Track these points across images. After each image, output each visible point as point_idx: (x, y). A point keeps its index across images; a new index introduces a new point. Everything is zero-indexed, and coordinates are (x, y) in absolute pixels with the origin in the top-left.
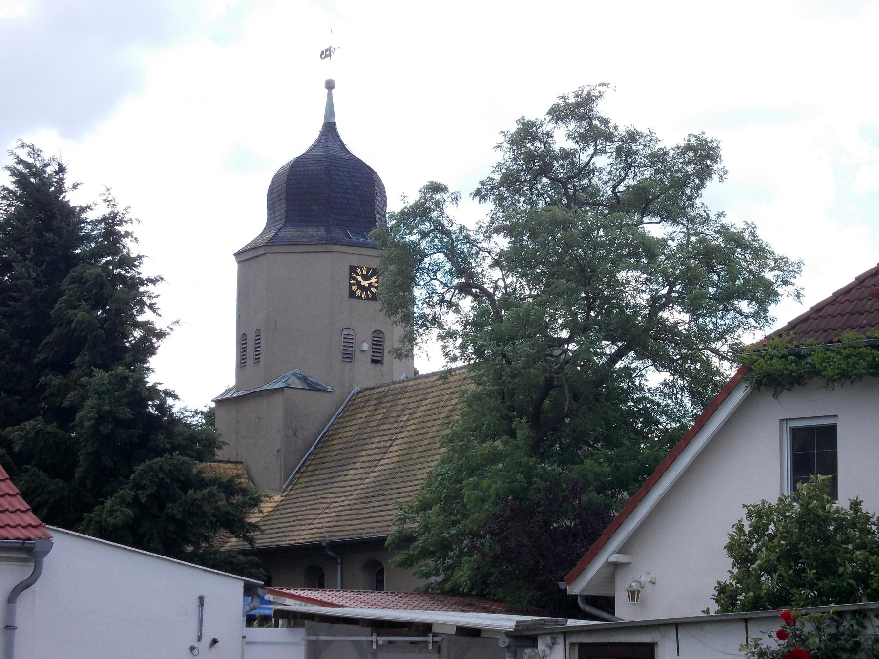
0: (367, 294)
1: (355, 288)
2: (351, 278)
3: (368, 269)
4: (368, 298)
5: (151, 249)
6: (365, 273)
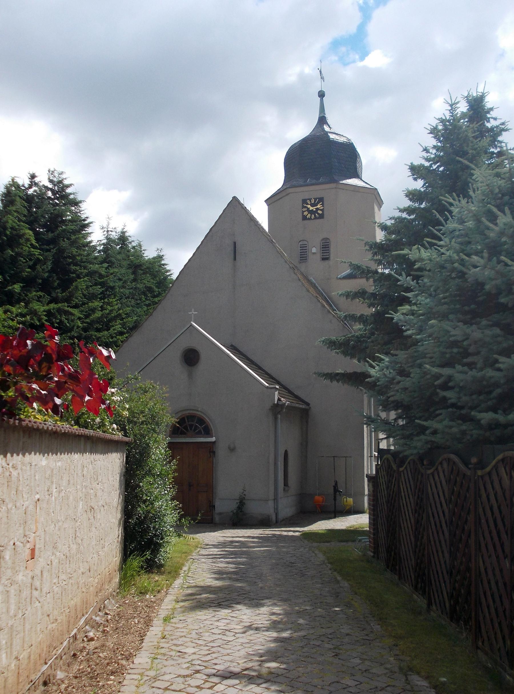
0: (315, 215)
1: (306, 213)
2: (304, 207)
3: (315, 199)
4: (316, 218)
5: (423, 163)
6: (313, 202)
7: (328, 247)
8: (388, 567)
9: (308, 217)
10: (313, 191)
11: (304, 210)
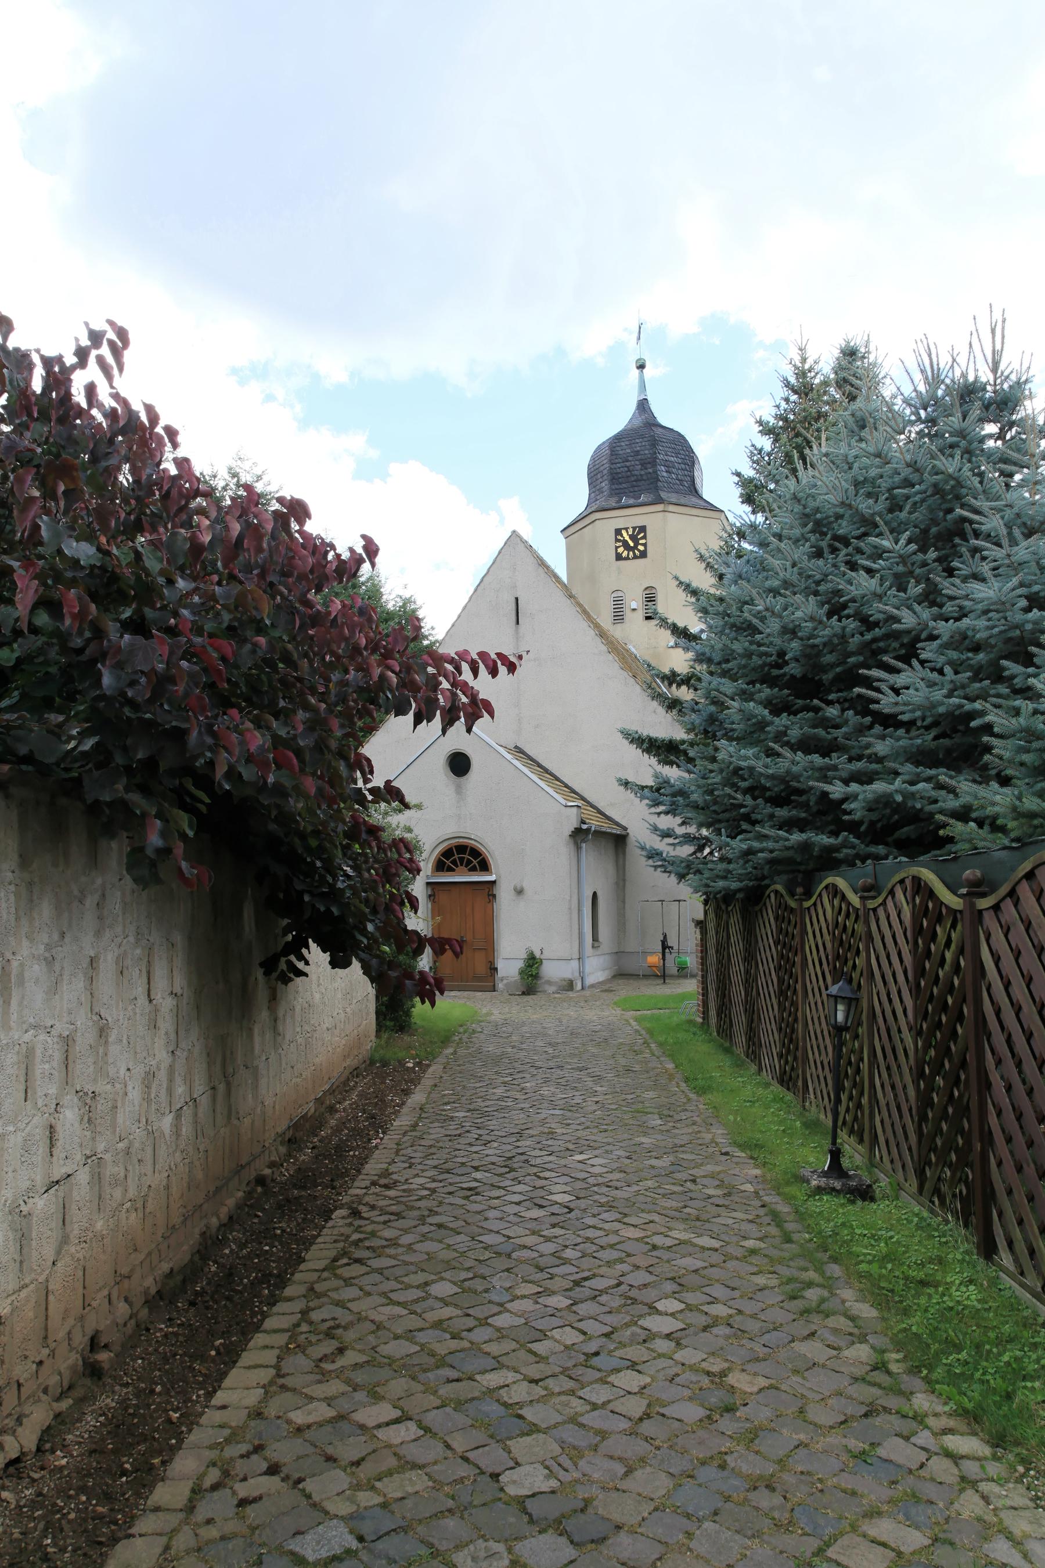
4: (635, 557)
10: (629, 519)
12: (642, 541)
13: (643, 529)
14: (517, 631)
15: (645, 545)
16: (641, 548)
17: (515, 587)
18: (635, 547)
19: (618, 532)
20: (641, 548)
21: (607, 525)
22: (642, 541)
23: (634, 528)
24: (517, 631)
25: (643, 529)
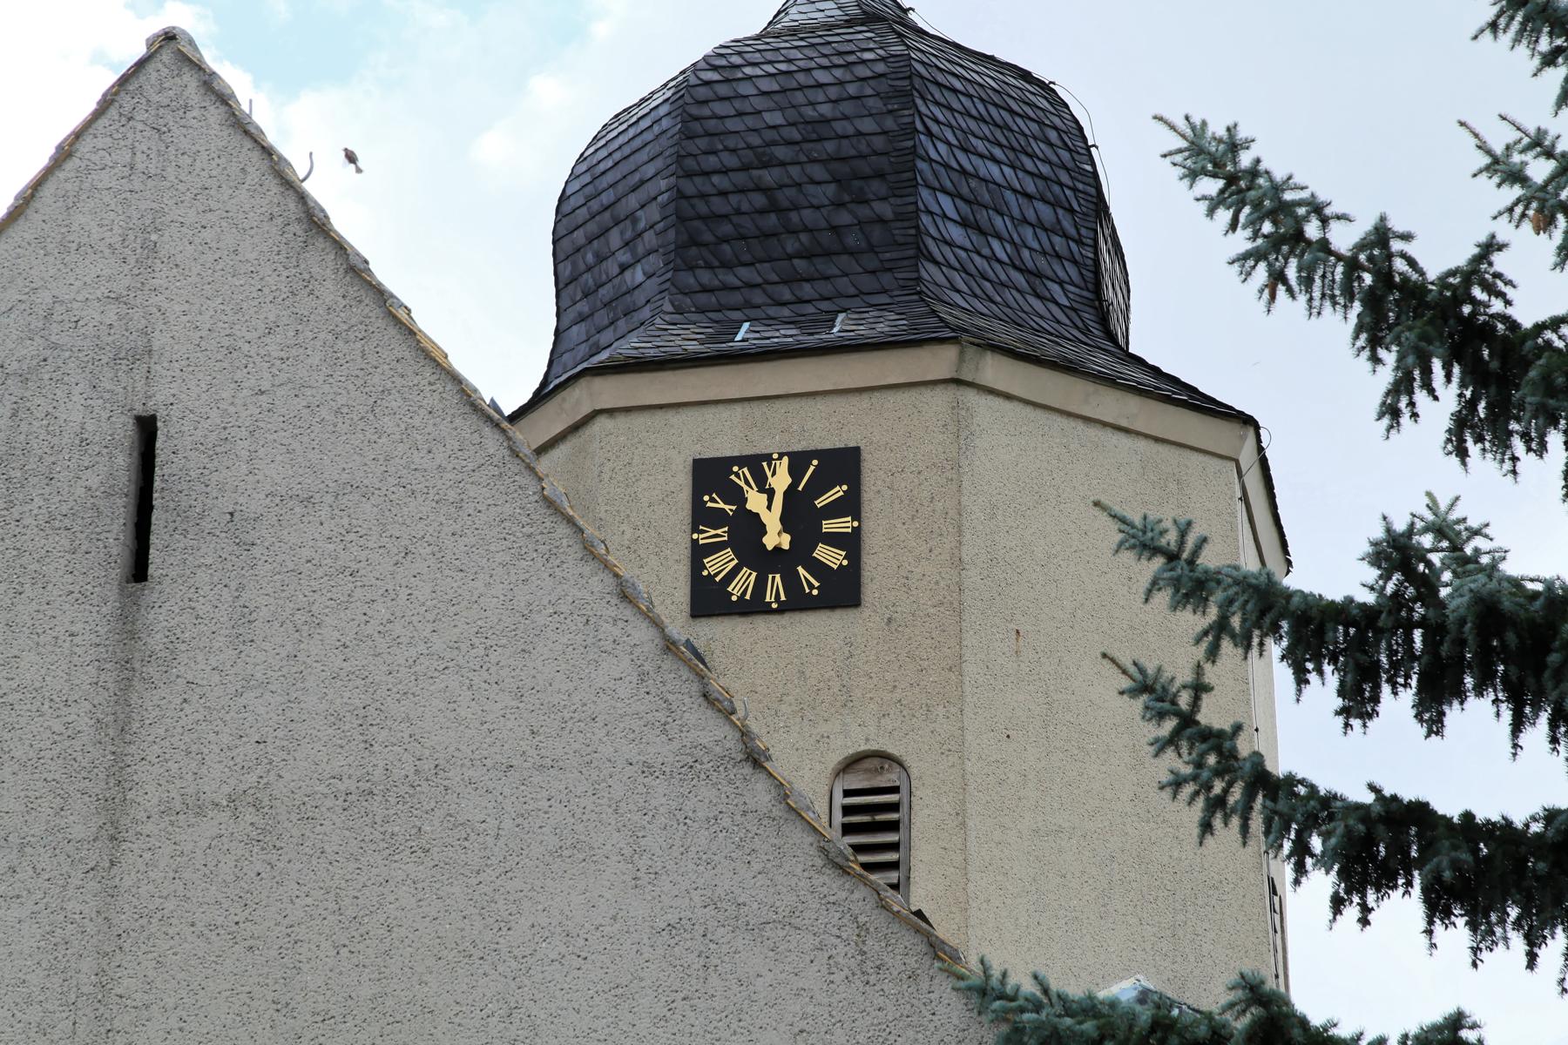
0: (792, 582)
4: (797, 602)
7: (894, 826)
8: (1440, 530)
9: (735, 590)
10: (772, 413)
11: (707, 536)
12: (840, 525)
13: (842, 465)
14: (128, 627)
15: (851, 543)
16: (831, 557)
17: (140, 355)
18: (801, 551)
19: (711, 475)
20: (831, 557)
21: (642, 465)
22: (840, 525)
23: (798, 462)
24: (128, 627)
25: (842, 465)
